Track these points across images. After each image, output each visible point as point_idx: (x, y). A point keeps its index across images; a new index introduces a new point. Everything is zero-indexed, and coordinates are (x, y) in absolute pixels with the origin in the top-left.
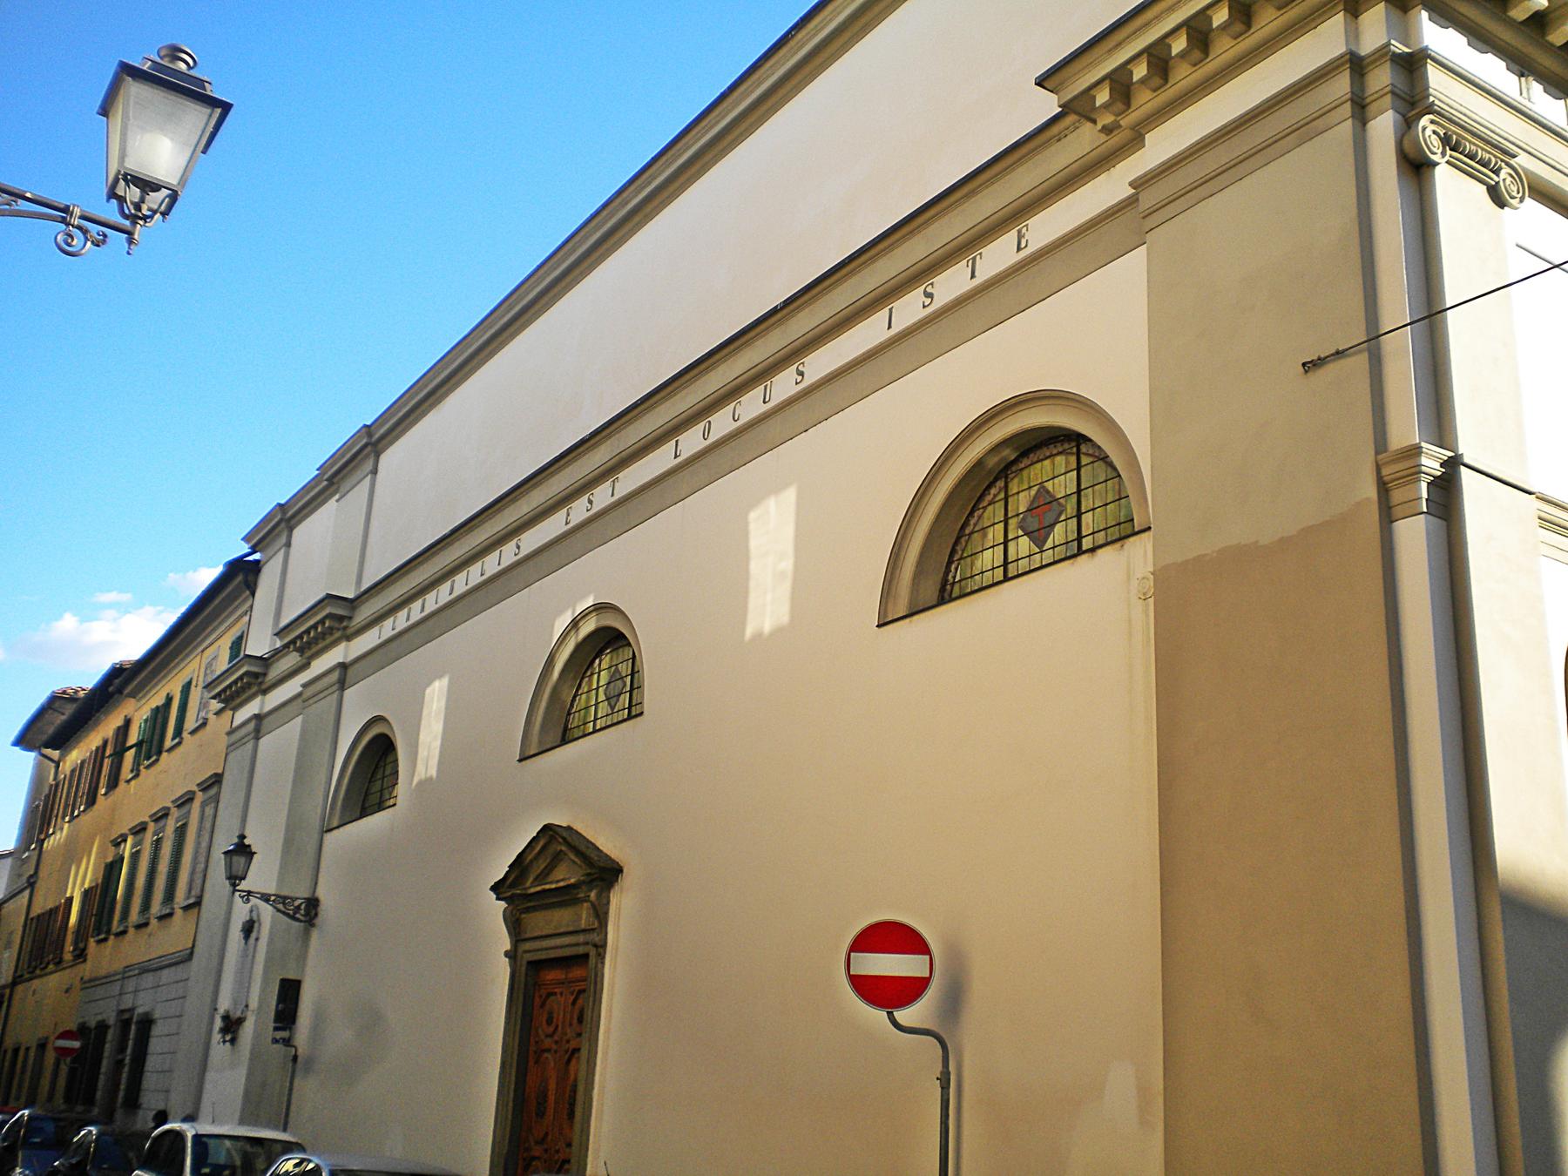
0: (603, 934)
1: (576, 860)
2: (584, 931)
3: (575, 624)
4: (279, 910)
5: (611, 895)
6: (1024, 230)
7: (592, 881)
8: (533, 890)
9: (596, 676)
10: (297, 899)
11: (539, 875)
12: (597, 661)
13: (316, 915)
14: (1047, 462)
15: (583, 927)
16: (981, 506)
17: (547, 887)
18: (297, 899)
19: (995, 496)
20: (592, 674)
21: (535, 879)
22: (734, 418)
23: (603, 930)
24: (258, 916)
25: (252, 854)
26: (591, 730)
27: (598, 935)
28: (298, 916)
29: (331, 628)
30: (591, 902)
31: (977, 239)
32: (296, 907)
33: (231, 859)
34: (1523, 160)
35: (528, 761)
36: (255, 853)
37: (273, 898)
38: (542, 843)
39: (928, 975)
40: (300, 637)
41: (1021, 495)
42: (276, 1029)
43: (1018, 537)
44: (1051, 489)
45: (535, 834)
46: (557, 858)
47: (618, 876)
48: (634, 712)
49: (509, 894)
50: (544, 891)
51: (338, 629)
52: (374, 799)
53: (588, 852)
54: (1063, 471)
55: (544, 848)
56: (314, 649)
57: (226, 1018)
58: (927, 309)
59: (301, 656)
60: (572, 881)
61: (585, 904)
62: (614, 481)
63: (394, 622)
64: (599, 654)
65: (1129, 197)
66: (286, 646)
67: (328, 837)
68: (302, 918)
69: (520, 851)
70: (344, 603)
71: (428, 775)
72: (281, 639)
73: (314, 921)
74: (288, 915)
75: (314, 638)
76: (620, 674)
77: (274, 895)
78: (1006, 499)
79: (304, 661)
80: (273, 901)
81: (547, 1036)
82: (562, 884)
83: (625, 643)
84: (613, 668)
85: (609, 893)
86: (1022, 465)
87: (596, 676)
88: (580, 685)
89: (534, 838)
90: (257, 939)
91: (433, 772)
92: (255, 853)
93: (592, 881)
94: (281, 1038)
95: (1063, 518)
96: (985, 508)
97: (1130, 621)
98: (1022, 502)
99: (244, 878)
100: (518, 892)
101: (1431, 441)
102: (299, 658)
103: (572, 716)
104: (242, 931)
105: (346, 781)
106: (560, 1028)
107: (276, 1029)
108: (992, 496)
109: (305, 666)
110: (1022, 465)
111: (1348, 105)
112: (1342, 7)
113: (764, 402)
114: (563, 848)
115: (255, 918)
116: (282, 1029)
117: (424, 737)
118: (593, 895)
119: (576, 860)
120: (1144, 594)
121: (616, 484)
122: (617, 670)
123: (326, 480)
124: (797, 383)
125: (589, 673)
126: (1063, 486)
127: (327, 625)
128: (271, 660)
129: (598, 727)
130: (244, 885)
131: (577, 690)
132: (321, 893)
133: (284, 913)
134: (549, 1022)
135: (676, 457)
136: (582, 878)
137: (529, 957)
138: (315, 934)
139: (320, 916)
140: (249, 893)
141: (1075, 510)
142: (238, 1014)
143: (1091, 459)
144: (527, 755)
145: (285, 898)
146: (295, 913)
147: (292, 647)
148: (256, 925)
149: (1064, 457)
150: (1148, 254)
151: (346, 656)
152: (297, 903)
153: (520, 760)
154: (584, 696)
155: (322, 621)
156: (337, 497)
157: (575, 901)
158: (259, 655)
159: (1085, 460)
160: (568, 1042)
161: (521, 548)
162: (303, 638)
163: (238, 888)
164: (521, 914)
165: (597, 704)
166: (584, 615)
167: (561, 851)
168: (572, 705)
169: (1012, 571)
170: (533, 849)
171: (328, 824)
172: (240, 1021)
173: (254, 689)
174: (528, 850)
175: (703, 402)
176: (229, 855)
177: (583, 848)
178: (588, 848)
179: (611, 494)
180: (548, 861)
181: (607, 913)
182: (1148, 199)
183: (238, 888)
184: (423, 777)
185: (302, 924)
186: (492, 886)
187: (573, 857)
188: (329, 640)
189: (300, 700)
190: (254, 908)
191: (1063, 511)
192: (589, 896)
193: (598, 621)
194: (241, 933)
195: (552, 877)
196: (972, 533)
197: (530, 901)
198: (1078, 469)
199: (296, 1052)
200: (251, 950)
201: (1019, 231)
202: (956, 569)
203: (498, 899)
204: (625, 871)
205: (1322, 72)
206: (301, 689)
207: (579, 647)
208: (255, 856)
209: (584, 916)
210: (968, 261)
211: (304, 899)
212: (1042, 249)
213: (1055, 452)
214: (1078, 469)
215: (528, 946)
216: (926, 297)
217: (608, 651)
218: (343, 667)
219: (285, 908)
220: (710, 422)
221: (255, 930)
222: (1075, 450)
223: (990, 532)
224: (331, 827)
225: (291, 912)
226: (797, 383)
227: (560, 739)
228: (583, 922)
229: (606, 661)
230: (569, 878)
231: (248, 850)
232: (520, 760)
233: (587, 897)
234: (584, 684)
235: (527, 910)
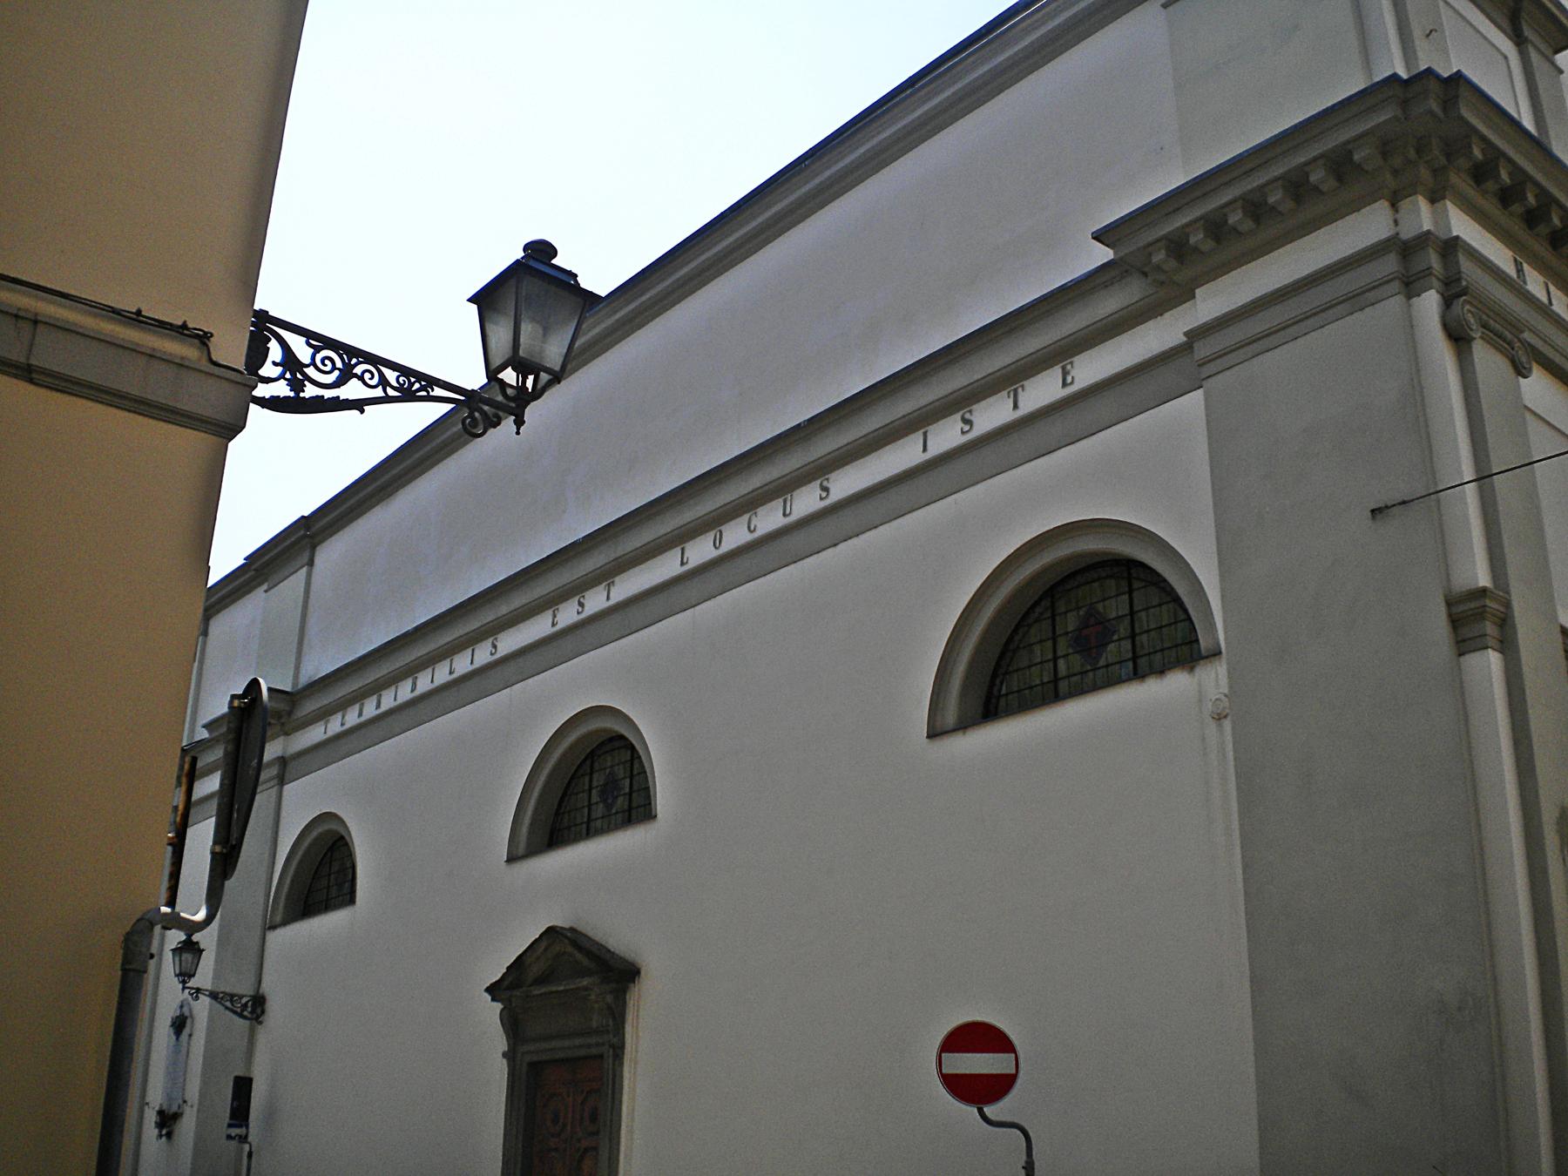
4: (227, 1008)
5: (628, 997)
6: (1069, 367)
10: (243, 996)
13: (263, 1012)
14: (1096, 585)
16: (1025, 624)
18: (243, 996)
19: (1041, 614)
22: (749, 527)
24: (191, 1011)
27: (614, 1036)
28: (245, 1013)
34: (1527, 336)
36: (203, 950)
37: (221, 995)
39: (1014, 1071)
41: (1069, 615)
42: (230, 1126)
43: (1068, 655)
45: (537, 936)
47: (635, 978)
54: (1113, 594)
57: (161, 1113)
62: (609, 585)
65: (1181, 346)
67: (273, 937)
72: (210, 732)
73: (260, 1019)
74: (235, 1012)
77: (222, 993)
78: (1053, 617)
80: (222, 998)
81: (553, 1136)
83: (950, 716)
86: (1068, 587)
89: (536, 940)
90: (190, 1035)
92: (203, 950)
94: (236, 1136)
95: (1115, 637)
96: (1030, 626)
97: (1203, 739)
98: (1071, 622)
99: (194, 975)
104: (172, 1026)
105: (288, 881)
106: (569, 1128)
107: (230, 1126)
108: (1036, 614)
110: (1068, 587)
113: (784, 515)
115: (187, 1014)
116: (240, 1126)
120: (1218, 714)
121: (612, 589)
123: (255, 570)
126: (1115, 608)
130: (192, 983)
132: (267, 987)
134: (555, 1121)
137: (528, 1058)
139: (266, 1013)
140: (198, 990)
141: (1129, 631)
142: (174, 1109)
143: (1143, 584)
146: (242, 1011)
148: (189, 1021)
150: (1206, 400)
152: (244, 1000)
156: (265, 587)
159: (1136, 585)
160: (579, 1140)
163: (187, 985)
169: (1063, 686)
171: (271, 921)
172: (176, 1116)
176: (178, 951)
178: (599, 949)
182: (1203, 350)
183: (187, 985)
185: (248, 1022)
190: (185, 1003)
191: (1115, 631)
194: (171, 1029)
196: (1018, 647)
198: (1130, 592)
199: (251, 1149)
200: (185, 1044)
201: (1064, 368)
202: (1002, 683)
203: (493, 1000)
210: (1009, 393)
211: (250, 996)
213: (1104, 574)
214: (1130, 592)
215: (525, 1048)
216: (964, 423)
219: (233, 1005)
220: (721, 532)
222: (1125, 575)
223: (1037, 649)
225: (239, 1010)
231: (196, 946)
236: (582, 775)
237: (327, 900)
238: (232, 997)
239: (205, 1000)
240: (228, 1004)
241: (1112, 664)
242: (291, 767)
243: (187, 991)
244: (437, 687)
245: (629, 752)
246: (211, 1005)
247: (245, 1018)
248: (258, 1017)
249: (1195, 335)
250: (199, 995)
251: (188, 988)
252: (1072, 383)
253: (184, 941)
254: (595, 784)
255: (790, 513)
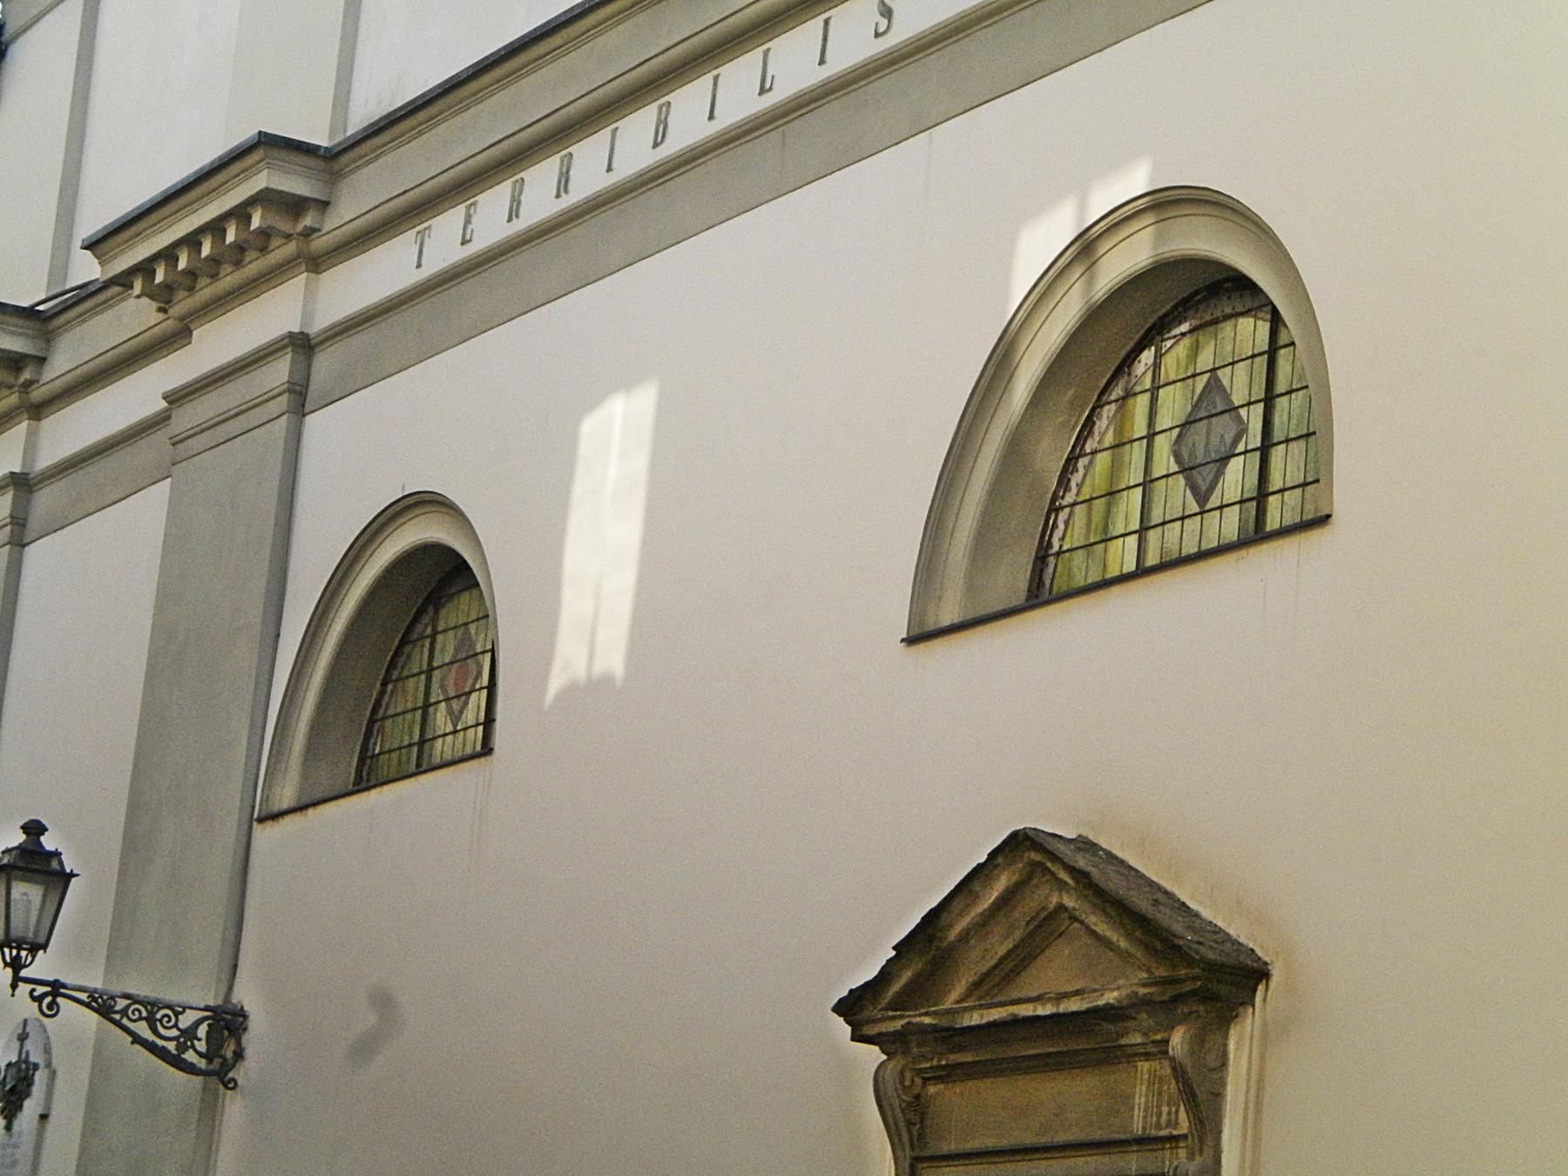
0: (1208, 1152)
1: (1113, 936)
2: (1144, 1142)
3: (1085, 247)
4: (137, 1039)
7: (1177, 999)
8: (975, 1019)
9: (1142, 402)
11: (985, 976)
12: (1147, 356)
13: (239, 1055)
15: (1137, 1127)
16: (1113, 397)
17: (1025, 1011)
20: (1129, 394)
21: (977, 985)
23: (1210, 1142)
25: (66, 878)
26: (1130, 566)
27: (1191, 1157)
28: (190, 1056)
29: (265, 234)
30: (1172, 1059)
31: (476, 177)
32: (183, 1032)
33: (1284, 484)
35: (938, 645)
36: (72, 875)
37: (121, 1004)
38: (1002, 882)
40: (168, 255)
44: (1226, 382)
46: (1046, 929)
48: (487, 749)
49: (898, 1025)
50: (1016, 1022)
51: (288, 237)
52: (401, 732)
53: (1164, 917)
55: (1007, 900)
56: (207, 291)
58: (881, 39)
59: (162, 310)
60: (1110, 997)
61: (1144, 1066)
63: (468, 221)
64: (1153, 334)
66: (123, 281)
68: (202, 1064)
69: (934, 905)
70: (312, 162)
71: (598, 668)
75: (210, 259)
76: (1227, 397)
77: (126, 996)
79: (170, 325)
80: (124, 1012)
82: (1074, 1005)
84: (1201, 382)
85: (1226, 1037)
87: (1142, 402)
88: (1089, 424)
89: (979, 869)
91: (613, 661)
92: (72, 875)
93: (1177, 999)
100: (927, 1020)
101: (60, 890)
102: (157, 317)
103: (1063, 516)
109: (178, 337)
111: (284, 398)
112: (304, 267)
114: (1070, 902)
117: (576, 557)
118: (1178, 1040)
119: (1113, 936)
122: (1214, 385)
124: (877, 35)
125: (1118, 392)
127: (256, 223)
128: (62, 319)
129: (1152, 559)
130: (41, 967)
131: (1081, 439)
132: (246, 995)
133: (151, 1048)
135: (763, 91)
136: (1142, 991)
138: (234, 1109)
140: (56, 988)
144: (931, 625)
145: (152, 1005)
146: (182, 1048)
147: (138, 286)
148: (40, 1078)
149: (1251, 320)
151: (307, 315)
152: (186, 1020)
153: (911, 640)
154: (1103, 459)
155: (240, 213)
157: (1111, 1056)
158: (25, 304)
161: (896, 16)
162: (249, 218)
163: (24, 973)
164: (925, 1080)
165: (1147, 484)
166: (1118, 220)
167: (1061, 907)
168: (1064, 482)
170: (976, 898)
171: (266, 799)
173: (281, 251)
174: (958, 904)
175: (116, 351)
177: (1143, 904)
178: (1156, 903)
179: (606, 166)
180: (1018, 935)
181: (1218, 1095)
183: (24, 973)
184: (580, 672)
185: (198, 1080)
186: (840, 1001)
187: (1102, 928)
188: (254, 265)
189: (161, 436)
192: (1166, 1042)
193: (1159, 238)
195: (1030, 983)
197: (961, 1049)
204: (1276, 976)
205: (261, 353)
206: (164, 404)
207: (1095, 317)
208: (73, 880)
209: (1140, 1100)
211: (206, 1009)
212: (490, 249)
217: (1184, 327)
218: (302, 345)
221: (38, 1089)
224: (277, 807)
225: (171, 1046)
226: (877, 35)
227: (1023, 585)
228: (1138, 1115)
229: (1176, 353)
230: (1102, 991)
232: (911, 640)
233: (1161, 1049)
234: (1101, 424)
235: (948, 1074)
236: (418, 639)
237: (422, 742)
238: (152, 1009)
239: (76, 1018)
240: (143, 1029)
241: (1170, 522)
242: (325, 364)
243: (24, 988)
244: (728, 131)
245: (1264, 328)
246: (99, 1023)
247: (190, 1069)
248: (226, 1067)
249: (176, 398)
250: (59, 1000)
251: (27, 981)
252: (470, 241)
253: (19, 847)
254: (1163, 421)
255: (771, 89)
